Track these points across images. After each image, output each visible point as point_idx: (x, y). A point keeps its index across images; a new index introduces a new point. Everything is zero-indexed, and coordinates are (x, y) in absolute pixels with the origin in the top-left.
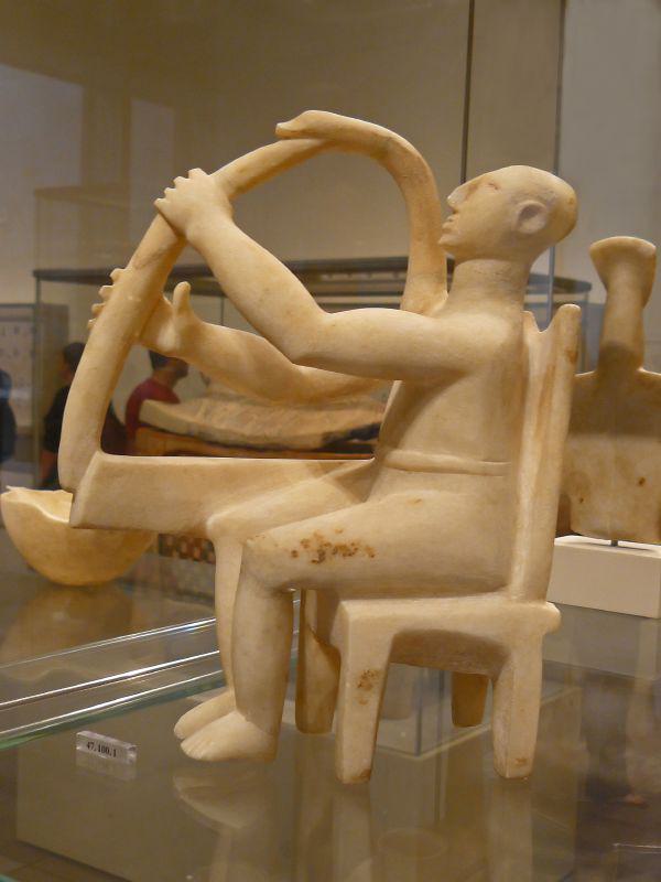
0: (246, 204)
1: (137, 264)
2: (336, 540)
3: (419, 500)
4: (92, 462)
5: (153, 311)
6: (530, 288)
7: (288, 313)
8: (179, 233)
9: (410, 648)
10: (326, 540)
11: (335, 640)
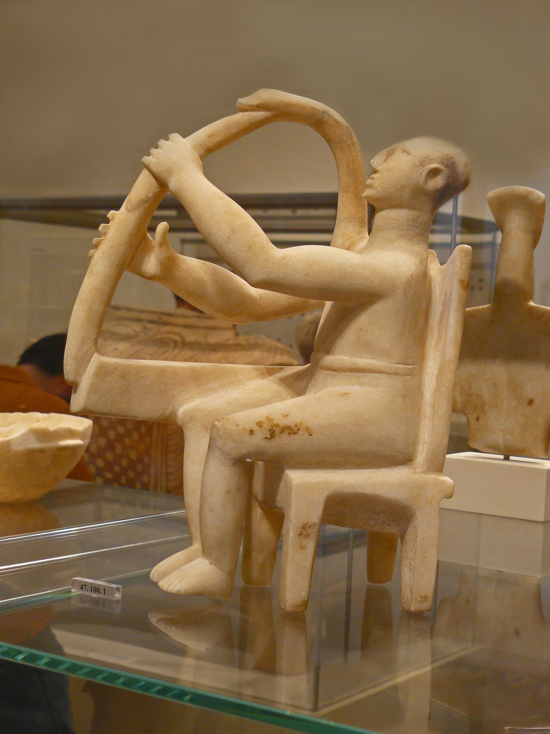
0: (210, 158)
1: (129, 207)
2: (283, 422)
3: (346, 394)
4: (92, 361)
5: (139, 245)
6: (437, 227)
7: (250, 247)
8: (162, 183)
9: (339, 506)
10: (275, 422)
11: (280, 500)
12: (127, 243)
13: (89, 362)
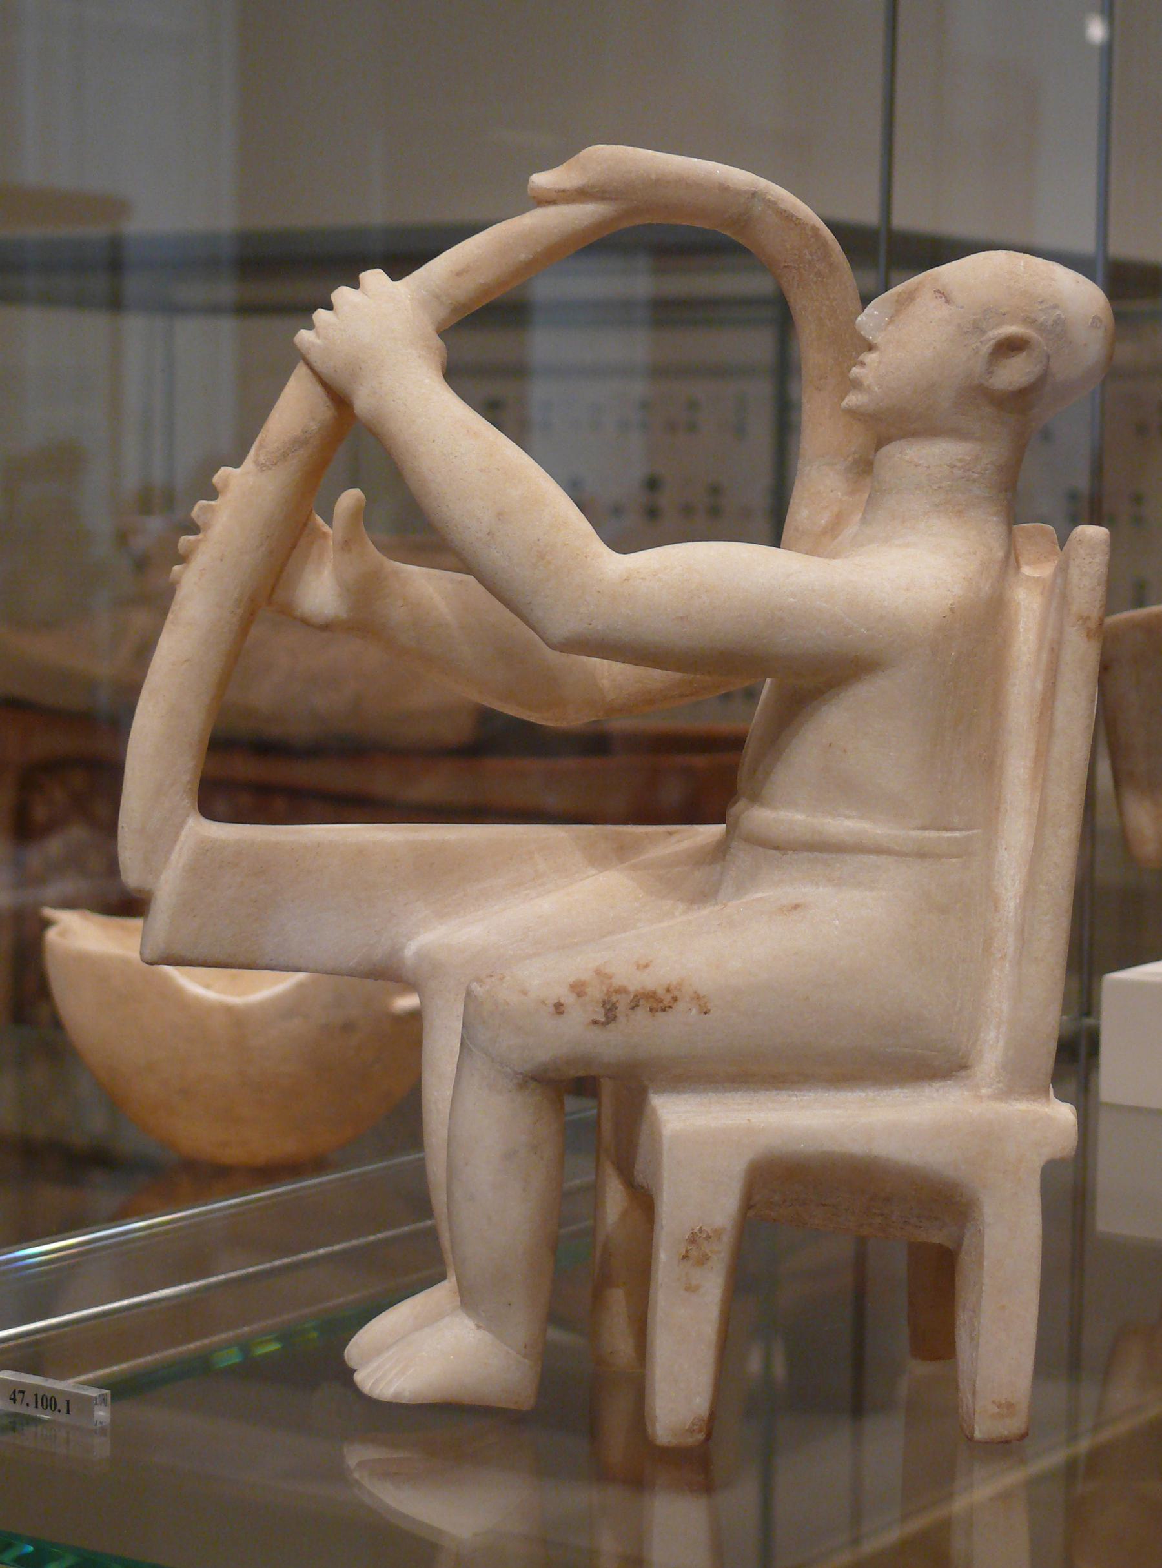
1: (262, 459)
3: (796, 907)
8: (339, 399)
10: (617, 982)
12: (262, 545)
13: (175, 841)
